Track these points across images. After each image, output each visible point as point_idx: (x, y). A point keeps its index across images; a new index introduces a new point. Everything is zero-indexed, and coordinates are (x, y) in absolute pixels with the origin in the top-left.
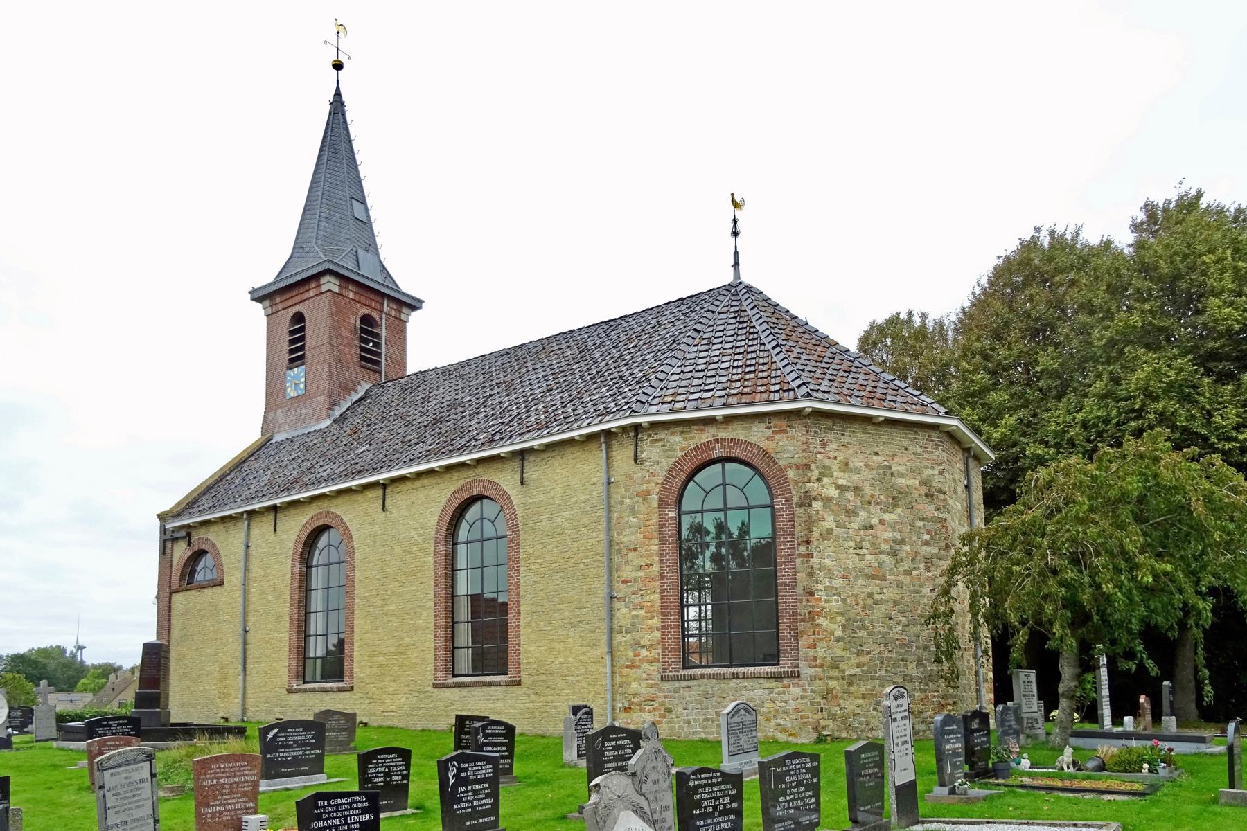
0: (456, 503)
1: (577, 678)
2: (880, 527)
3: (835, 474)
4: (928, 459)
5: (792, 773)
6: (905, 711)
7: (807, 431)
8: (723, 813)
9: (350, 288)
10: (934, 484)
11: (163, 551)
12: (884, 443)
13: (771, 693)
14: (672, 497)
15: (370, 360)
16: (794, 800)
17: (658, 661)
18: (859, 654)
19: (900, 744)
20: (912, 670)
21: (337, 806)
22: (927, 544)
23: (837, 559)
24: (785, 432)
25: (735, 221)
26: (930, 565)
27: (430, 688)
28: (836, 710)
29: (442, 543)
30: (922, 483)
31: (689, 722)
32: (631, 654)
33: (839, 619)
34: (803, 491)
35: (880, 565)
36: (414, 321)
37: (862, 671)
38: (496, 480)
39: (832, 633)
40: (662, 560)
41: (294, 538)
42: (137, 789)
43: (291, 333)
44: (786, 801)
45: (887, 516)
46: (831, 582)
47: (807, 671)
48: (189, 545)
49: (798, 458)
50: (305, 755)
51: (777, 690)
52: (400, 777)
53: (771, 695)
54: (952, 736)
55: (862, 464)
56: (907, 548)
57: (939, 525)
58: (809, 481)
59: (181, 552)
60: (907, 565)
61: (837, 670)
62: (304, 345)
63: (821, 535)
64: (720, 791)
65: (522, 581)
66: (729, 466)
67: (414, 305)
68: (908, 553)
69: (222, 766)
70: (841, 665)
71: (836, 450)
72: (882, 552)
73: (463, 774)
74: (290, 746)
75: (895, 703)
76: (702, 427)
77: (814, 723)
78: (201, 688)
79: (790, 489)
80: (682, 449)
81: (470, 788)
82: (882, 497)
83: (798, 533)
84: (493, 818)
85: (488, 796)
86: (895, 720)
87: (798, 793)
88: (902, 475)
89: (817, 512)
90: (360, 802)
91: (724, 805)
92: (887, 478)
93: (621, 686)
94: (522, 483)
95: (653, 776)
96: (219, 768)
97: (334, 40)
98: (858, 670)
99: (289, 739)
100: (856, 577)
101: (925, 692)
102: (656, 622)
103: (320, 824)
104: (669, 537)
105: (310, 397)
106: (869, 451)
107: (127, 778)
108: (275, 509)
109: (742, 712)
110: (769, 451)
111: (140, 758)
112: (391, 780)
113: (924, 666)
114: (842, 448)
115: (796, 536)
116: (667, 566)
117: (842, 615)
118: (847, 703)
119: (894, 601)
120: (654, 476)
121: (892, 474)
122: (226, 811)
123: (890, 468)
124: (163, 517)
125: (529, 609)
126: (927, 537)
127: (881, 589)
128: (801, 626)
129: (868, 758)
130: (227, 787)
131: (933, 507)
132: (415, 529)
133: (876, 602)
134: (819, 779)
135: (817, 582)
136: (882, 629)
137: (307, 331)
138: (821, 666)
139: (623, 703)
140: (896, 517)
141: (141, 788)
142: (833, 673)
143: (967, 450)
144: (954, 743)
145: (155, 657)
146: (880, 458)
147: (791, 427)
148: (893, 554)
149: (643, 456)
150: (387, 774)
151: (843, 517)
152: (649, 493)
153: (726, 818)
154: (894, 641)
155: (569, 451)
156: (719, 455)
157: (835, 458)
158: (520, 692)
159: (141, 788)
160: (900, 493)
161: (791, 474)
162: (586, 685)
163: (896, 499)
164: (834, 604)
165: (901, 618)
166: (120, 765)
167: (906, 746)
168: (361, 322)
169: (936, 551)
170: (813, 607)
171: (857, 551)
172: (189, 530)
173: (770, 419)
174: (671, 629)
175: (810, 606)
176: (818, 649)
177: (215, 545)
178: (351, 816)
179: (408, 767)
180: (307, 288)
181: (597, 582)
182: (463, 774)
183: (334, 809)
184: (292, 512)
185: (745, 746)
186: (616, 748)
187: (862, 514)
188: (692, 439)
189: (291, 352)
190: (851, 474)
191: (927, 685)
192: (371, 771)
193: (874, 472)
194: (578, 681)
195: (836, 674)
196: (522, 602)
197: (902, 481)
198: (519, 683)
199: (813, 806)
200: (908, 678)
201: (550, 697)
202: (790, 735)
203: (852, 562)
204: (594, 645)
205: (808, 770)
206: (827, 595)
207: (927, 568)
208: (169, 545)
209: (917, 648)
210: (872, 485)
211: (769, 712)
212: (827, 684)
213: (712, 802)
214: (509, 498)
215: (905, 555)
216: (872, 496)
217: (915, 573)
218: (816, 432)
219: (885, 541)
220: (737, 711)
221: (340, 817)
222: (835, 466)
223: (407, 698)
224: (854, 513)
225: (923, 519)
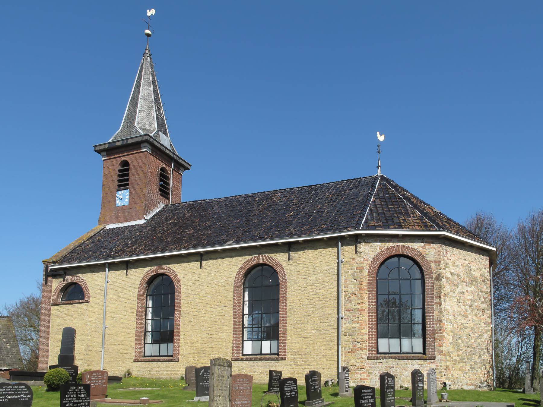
2: (466, 293)
4: (483, 265)
10: (486, 276)
13: (422, 366)
18: (458, 350)
20: (477, 359)
22: (483, 303)
26: (484, 312)
28: (449, 375)
30: (481, 275)
32: (351, 346)
33: (451, 334)
34: (438, 273)
39: (448, 340)
40: (370, 301)
43: (120, 171)
45: (469, 289)
46: (448, 316)
49: (436, 258)
51: (424, 365)
53: (422, 368)
55: (460, 264)
56: (476, 304)
61: (450, 357)
63: (445, 294)
65: (288, 308)
71: (451, 256)
72: (467, 305)
76: (390, 239)
82: (467, 280)
88: (474, 271)
98: (458, 357)
100: (458, 315)
101: (482, 369)
104: (373, 290)
110: (422, 253)
113: (481, 357)
114: (453, 255)
115: (434, 294)
116: (371, 304)
117: (452, 332)
119: (471, 328)
120: (366, 260)
121: (471, 270)
123: (470, 267)
124: (47, 264)
126: (483, 300)
128: (436, 336)
133: (465, 327)
135: (443, 316)
136: (467, 340)
138: (445, 355)
142: (449, 358)
146: (467, 262)
148: (471, 306)
157: (451, 260)
161: (433, 265)
165: (473, 335)
168: (161, 170)
169: (486, 306)
171: (458, 303)
172: (64, 272)
173: (423, 238)
174: (373, 334)
176: (443, 347)
181: (333, 310)
192: (286, 389)
193: (464, 268)
198: (284, 359)
200: (476, 363)
203: (456, 308)
207: (483, 314)
210: (464, 274)
214: (281, 266)
224: (456, 286)
225: (482, 292)
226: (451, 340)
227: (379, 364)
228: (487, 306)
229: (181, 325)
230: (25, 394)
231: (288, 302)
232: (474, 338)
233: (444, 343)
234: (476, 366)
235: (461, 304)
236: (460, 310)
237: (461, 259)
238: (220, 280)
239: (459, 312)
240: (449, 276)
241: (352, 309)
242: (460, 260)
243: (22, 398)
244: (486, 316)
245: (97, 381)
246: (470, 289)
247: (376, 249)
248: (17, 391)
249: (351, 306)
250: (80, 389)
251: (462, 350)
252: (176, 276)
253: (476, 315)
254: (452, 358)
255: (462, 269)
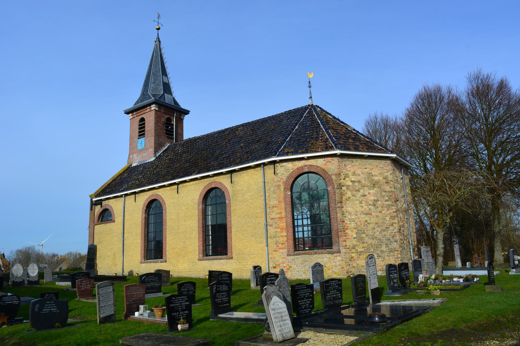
0: (206, 190)
1: (255, 256)
3: (350, 176)
5: (332, 285)
6: (374, 263)
7: (339, 161)
8: (307, 298)
9: (162, 108)
11: (91, 209)
12: (368, 164)
13: (330, 259)
14: (289, 187)
15: (169, 134)
16: (333, 294)
17: (286, 248)
18: (363, 243)
19: (372, 275)
21: (178, 299)
22: (387, 201)
23: (353, 208)
24: (330, 162)
25: (309, 82)
27: (197, 261)
28: (355, 265)
29: (201, 205)
30: (384, 178)
31: (298, 271)
33: (354, 230)
35: (370, 209)
36: (186, 119)
37: (365, 250)
38: (221, 181)
39: (352, 236)
41: (143, 204)
42: (109, 295)
44: (330, 295)
46: (351, 217)
47: (343, 250)
48: (101, 207)
50: (155, 286)
51: (332, 258)
52: (192, 292)
54: (392, 272)
56: (379, 203)
57: (391, 193)
58: (340, 180)
59: (98, 209)
60: (380, 209)
61: (355, 250)
62: (144, 130)
64: (306, 291)
66: (310, 174)
67: (187, 112)
68: (380, 204)
69: (133, 288)
70: (356, 248)
71: (350, 168)
72: (370, 205)
73: (218, 289)
74: (150, 282)
75: (370, 260)
77: (347, 270)
78: (106, 262)
79: (333, 183)
80: (292, 169)
81: (220, 294)
83: (337, 199)
84: (228, 304)
85: (226, 297)
86: (370, 266)
87: (334, 292)
88: (376, 176)
89: (344, 191)
90: (185, 298)
91: (308, 295)
92: (370, 177)
93: (271, 258)
94: (231, 183)
95: (283, 286)
96: (132, 289)
97: (157, 20)
99: (149, 280)
100: (360, 214)
102: (284, 234)
103: (173, 305)
105: (147, 149)
106: (363, 167)
107: (106, 291)
108: (135, 193)
109: (318, 266)
111: (110, 284)
112: (189, 293)
113: (388, 247)
117: (355, 229)
118: (359, 262)
119: (376, 223)
121: (372, 175)
122: (135, 303)
125: (235, 230)
127: (370, 218)
128: (340, 234)
129: (359, 280)
130: (135, 295)
131: (389, 187)
132: (190, 200)
133: (369, 223)
134: (342, 287)
135: (345, 217)
137: (146, 125)
138: (349, 248)
139: (273, 265)
140: (375, 191)
141: (110, 295)
142: (353, 251)
143: (402, 164)
144: (394, 274)
145: (92, 250)
146: (367, 170)
147: (333, 160)
148: (374, 205)
149: (278, 172)
150: (188, 291)
151: (354, 192)
152: (280, 186)
153: (308, 300)
154: (376, 238)
155: (249, 171)
156: (306, 171)
157: (350, 171)
158: (232, 262)
159: (110, 295)
160: (375, 182)
161: (334, 177)
162: (258, 258)
163: (374, 184)
164: (353, 225)
166: (104, 287)
167: (374, 275)
170: (344, 226)
171: (360, 205)
172: (99, 202)
175: (343, 226)
176: (347, 242)
177: (111, 207)
178: (182, 303)
179: (195, 289)
180: (146, 109)
182: (218, 289)
183: (177, 300)
184: (142, 194)
185: (319, 279)
186: (270, 280)
187: (362, 191)
188: (296, 165)
189: (139, 132)
190: (356, 176)
191: (390, 254)
194: (255, 257)
195: (354, 251)
196: (232, 227)
197: (376, 178)
198: (232, 258)
199: (340, 297)
201: (244, 263)
202: (338, 275)
203: (359, 209)
204: (261, 243)
205: (337, 285)
206: (349, 222)
207: (388, 210)
208: (93, 206)
209: (385, 240)
211: (329, 267)
212: (351, 255)
213: (303, 295)
214: (226, 188)
215: (379, 205)
216: (365, 184)
217: (383, 212)
218: (342, 161)
219: (371, 200)
220: (316, 266)
221: (179, 303)
222: (350, 174)
223: (188, 265)
224: (358, 191)
225: (385, 192)
226: (355, 236)
227: (296, 260)
228: (392, 203)
229: (167, 236)
230: (16, 301)
231: (232, 215)
232: (379, 231)
233: (348, 238)
234: (383, 255)
235: (363, 205)
236: (363, 209)
237: (361, 168)
238: (189, 202)
239: (362, 212)
240: (350, 184)
241: (274, 217)
242: (360, 170)
243: (14, 303)
244: (392, 211)
245: (86, 286)
246: (372, 191)
247: (289, 170)
248: (12, 299)
249: (274, 215)
250: (52, 296)
251: (367, 243)
252: (163, 200)
253: (381, 212)
254: (357, 250)
255: (362, 176)
